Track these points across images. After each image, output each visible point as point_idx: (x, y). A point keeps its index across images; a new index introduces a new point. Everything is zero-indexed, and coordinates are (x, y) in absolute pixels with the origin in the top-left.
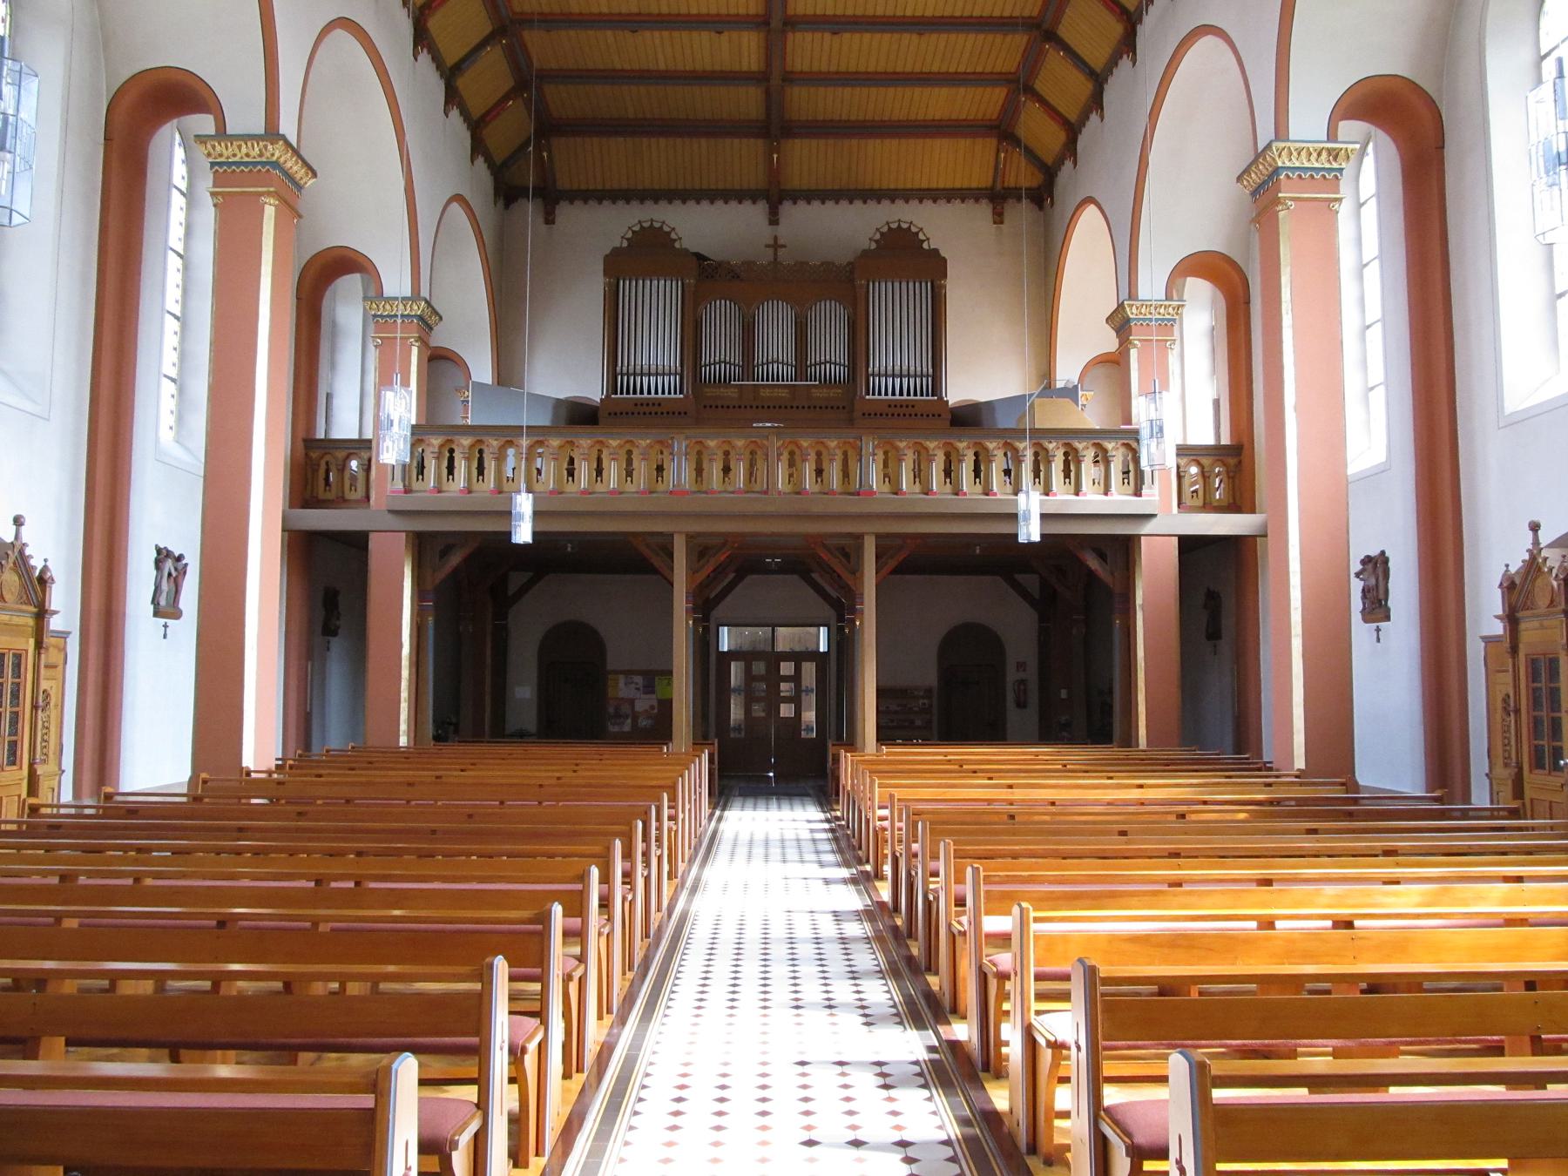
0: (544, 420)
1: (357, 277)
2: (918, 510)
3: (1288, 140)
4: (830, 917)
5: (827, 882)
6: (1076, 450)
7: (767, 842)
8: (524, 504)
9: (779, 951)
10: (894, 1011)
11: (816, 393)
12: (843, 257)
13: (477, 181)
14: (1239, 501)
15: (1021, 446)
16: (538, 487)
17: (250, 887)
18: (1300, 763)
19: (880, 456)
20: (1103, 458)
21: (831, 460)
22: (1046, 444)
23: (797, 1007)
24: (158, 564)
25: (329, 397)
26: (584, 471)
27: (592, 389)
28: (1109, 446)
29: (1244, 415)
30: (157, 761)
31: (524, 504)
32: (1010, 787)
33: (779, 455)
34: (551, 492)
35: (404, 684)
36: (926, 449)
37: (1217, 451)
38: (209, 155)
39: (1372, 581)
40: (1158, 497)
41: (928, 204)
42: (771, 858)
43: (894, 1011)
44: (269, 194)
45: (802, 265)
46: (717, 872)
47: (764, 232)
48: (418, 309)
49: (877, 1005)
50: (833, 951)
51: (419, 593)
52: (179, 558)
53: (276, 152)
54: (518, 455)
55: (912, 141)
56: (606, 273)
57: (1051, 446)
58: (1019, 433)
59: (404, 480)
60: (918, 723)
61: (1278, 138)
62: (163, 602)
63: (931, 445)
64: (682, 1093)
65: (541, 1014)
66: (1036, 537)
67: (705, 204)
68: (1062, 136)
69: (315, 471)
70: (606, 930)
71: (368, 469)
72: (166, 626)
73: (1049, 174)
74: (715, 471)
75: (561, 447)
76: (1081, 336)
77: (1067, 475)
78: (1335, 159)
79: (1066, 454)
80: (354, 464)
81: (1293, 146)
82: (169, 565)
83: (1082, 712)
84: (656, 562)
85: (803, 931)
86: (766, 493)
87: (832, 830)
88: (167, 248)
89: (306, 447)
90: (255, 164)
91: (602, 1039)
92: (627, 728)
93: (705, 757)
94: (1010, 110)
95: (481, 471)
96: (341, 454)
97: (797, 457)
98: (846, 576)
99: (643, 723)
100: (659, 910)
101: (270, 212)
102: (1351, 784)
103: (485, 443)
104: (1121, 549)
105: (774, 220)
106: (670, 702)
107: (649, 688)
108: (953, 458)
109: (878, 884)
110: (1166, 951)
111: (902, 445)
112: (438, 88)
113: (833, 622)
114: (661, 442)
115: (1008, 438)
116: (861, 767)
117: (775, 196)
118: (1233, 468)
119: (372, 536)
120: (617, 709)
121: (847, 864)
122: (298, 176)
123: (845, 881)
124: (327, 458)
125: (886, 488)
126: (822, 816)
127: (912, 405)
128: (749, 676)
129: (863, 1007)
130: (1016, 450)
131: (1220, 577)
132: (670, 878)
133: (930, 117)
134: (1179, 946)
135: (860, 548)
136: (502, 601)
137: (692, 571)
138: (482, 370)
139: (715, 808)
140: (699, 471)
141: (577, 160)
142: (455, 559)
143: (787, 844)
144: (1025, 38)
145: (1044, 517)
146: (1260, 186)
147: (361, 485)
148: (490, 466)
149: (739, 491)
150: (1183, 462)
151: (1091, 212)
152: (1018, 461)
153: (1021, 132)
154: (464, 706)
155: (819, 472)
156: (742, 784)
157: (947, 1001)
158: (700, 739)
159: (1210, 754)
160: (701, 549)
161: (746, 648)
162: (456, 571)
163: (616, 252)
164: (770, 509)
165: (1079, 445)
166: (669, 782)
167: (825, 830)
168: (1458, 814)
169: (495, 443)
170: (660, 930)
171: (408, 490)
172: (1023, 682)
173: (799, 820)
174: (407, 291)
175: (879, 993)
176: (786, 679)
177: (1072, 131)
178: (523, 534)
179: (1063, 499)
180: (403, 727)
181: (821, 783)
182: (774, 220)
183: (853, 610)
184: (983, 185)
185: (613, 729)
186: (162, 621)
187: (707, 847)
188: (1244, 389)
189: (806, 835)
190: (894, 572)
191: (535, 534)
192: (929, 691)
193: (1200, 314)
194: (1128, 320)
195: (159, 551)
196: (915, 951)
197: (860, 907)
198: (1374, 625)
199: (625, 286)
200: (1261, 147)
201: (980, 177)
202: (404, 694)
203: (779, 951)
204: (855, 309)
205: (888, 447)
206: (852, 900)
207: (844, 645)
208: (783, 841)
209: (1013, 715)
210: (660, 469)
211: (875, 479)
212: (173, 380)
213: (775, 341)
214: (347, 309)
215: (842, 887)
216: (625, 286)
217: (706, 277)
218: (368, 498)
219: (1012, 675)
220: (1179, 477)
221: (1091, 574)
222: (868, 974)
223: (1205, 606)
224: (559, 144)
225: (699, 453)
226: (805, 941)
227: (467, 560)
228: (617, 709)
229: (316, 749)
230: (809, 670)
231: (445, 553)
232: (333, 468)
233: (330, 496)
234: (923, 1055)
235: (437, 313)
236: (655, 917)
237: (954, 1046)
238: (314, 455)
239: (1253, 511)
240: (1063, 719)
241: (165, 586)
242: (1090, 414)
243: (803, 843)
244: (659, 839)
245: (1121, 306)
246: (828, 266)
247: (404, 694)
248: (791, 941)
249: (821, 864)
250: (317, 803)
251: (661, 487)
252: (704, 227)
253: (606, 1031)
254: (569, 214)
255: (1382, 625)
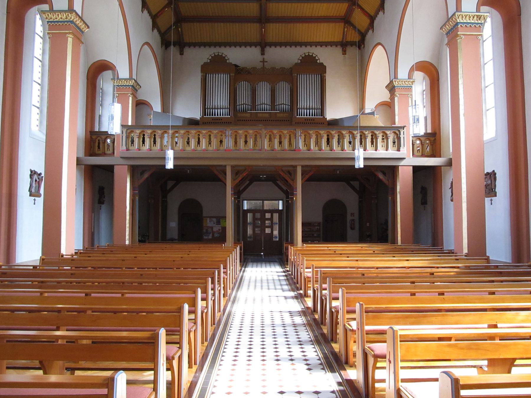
0: (180, 123)
1: (110, 72)
2: (318, 156)
3: (461, 12)
4: (288, 314)
5: (286, 298)
6: (376, 134)
7: (262, 281)
8: (170, 154)
9: (268, 331)
10: (319, 362)
11: (278, 115)
12: (287, 66)
13: (155, 38)
14: (435, 153)
15: (355, 132)
16: (176, 148)
17: (65, 298)
18: (465, 251)
19: (303, 137)
20: (385, 137)
21: (285, 138)
22: (365, 132)
23: (278, 360)
24: (31, 176)
25: (100, 116)
26: (193, 142)
27: (197, 115)
28: (388, 132)
29: (437, 121)
30: (29, 250)
31: (170, 154)
32: (357, 261)
33: (266, 136)
34: (181, 150)
35: (127, 221)
36: (320, 134)
37: (427, 135)
38: (47, 18)
39: (489, 182)
40: (406, 151)
41: (319, 47)
42: (264, 287)
43: (319, 362)
44: (69, 33)
45: (273, 69)
46: (243, 294)
47: (260, 58)
48: (131, 83)
49: (313, 358)
50: (290, 330)
51: (133, 188)
52: (40, 174)
53: (72, 17)
54: (168, 136)
55: (313, 24)
56: (202, 71)
57: (366, 133)
58: (356, 128)
59: (126, 146)
60: (315, 235)
61: (395, 78)
62: (33, 190)
63: (322, 132)
64: (235, 358)
65: (179, 343)
66: (362, 166)
67: (238, 47)
68: (367, 21)
69: (94, 143)
70: (213, 299)
71: (114, 143)
72: (35, 200)
73: (363, 36)
74: (242, 142)
75: (184, 133)
76: (375, 92)
77: (372, 143)
78: (480, 19)
79: (372, 136)
80: (109, 141)
81: (463, 14)
82: (35, 177)
83: (376, 231)
84: (220, 176)
85: (278, 321)
86: (261, 150)
87: (286, 276)
88: (33, 57)
89: (91, 134)
90: (64, 22)
91: (191, 380)
92: (210, 237)
93: (238, 248)
94: (349, 12)
95: (155, 142)
96: (104, 137)
97: (272, 137)
98: (290, 182)
99: (216, 235)
100: (219, 311)
101: (70, 40)
102: (488, 260)
103: (156, 133)
104: (391, 171)
105: (263, 54)
106: (226, 227)
107: (218, 223)
108: (330, 137)
109: (306, 299)
110: (465, 351)
111: (311, 132)
112: (150, 21)
113: (285, 199)
114: (221, 131)
115: (351, 129)
116: (298, 252)
117: (263, 45)
118: (432, 142)
119: (115, 167)
120: (207, 230)
121: (293, 290)
122: (82, 27)
123: (293, 298)
124: (99, 138)
125: (305, 148)
126: (281, 270)
127: (314, 119)
128: (254, 219)
129: (306, 360)
130: (353, 134)
131: (427, 181)
132: (224, 297)
133: (319, 15)
134: (471, 349)
135: (295, 171)
136: (165, 192)
137: (233, 179)
138: (157, 107)
139: (242, 267)
140: (236, 142)
141: (191, 31)
142: (146, 176)
143: (269, 281)
144: (347, 4)
145: (365, 159)
146: (450, 31)
147: (111, 148)
148: (158, 140)
149: (251, 150)
150: (414, 139)
151: (379, 49)
152: (354, 138)
153: (352, 20)
154: (149, 230)
155: (280, 143)
156: (252, 257)
157: (343, 358)
158: (237, 241)
159: (422, 247)
160: (236, 171)
161: (253, 208)
162: (147, 178)
163: (205, 64)
164: (262, 156)
165: (377, 132)
166: (224, 260)
167: (283, 276)
168: (493, 267)
169: (160, 132)
170: (220, 321)
171: (128, 150)
172: (353, 220)
173: (272, 272)
174: (127, 76)
175: (312, 352)
176: (268, 219)
177: (372, 19)
178: (170, 165)
179: (371, 152)
180: (127, 237)
181: (281, 257)
182: (263, 54)
183: (293, 194)
184: (338, 40)
185: (205, 237)
186: (33, 198)
187: (239, 283)
188: (437, 113)
189: (276, 278)
190: (306, 181)
191: (174, 166)
192: (319, 224)
193: (420, 87)
194: (394, 87)
195: (31, 171)
196: (325, 331)
197: (300, 310)
198: (490, 198)
199: (209, 76)
200: (449, 16)
201: (338, 38)
202: (127, 225)
203: (268, 331)
204: (293, 85)
205: (306, 133)
206: (297, 306)
207: (289, 207)
208: (268, 280)
209: (350, 232)
210: (221, 142)
211: (301, 145)
212: (38, 108)
213: (264, 96)
214: (106, 85)
215: (292, 300)
216: (209, 76)
217: (238, 73)
218: (114, 153)
219: (349, 218)
220: (413, 145)
221: (380, 180)
222: (306, 342)
223: (421, 192)
224: (186, 27)
225: (236, 136)
226: (279, 326)
227: (151, 175)
228: (207, 230)
229: (96, 244)
230: (276, 216)
231: (142, 173)
232: (101, 142)
233: (100, 152)
234: (336, 388)
235: (139, 85)
236: (218, 315)
237: (350, 383)
238: (94, 137)
239: (440, 157)
240: (368, 234)
241: (34, 185)
242: (379, 121)
243: (275, 281)
244: (219, 281)
245: (391, 82)
246: (283, 69)
247: (127, 225)
248: (273, 326)
249: (283, 290)
250: (86, 269)
251: (221, 148)
252: (237, 56)
253: (193, 375)
254: (188, 51)
255: (493, 198)
